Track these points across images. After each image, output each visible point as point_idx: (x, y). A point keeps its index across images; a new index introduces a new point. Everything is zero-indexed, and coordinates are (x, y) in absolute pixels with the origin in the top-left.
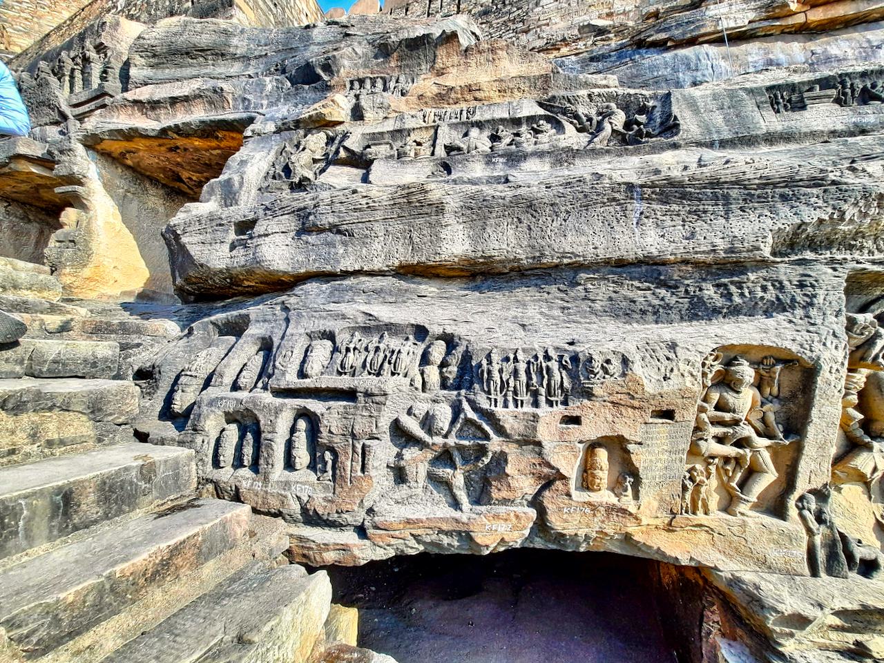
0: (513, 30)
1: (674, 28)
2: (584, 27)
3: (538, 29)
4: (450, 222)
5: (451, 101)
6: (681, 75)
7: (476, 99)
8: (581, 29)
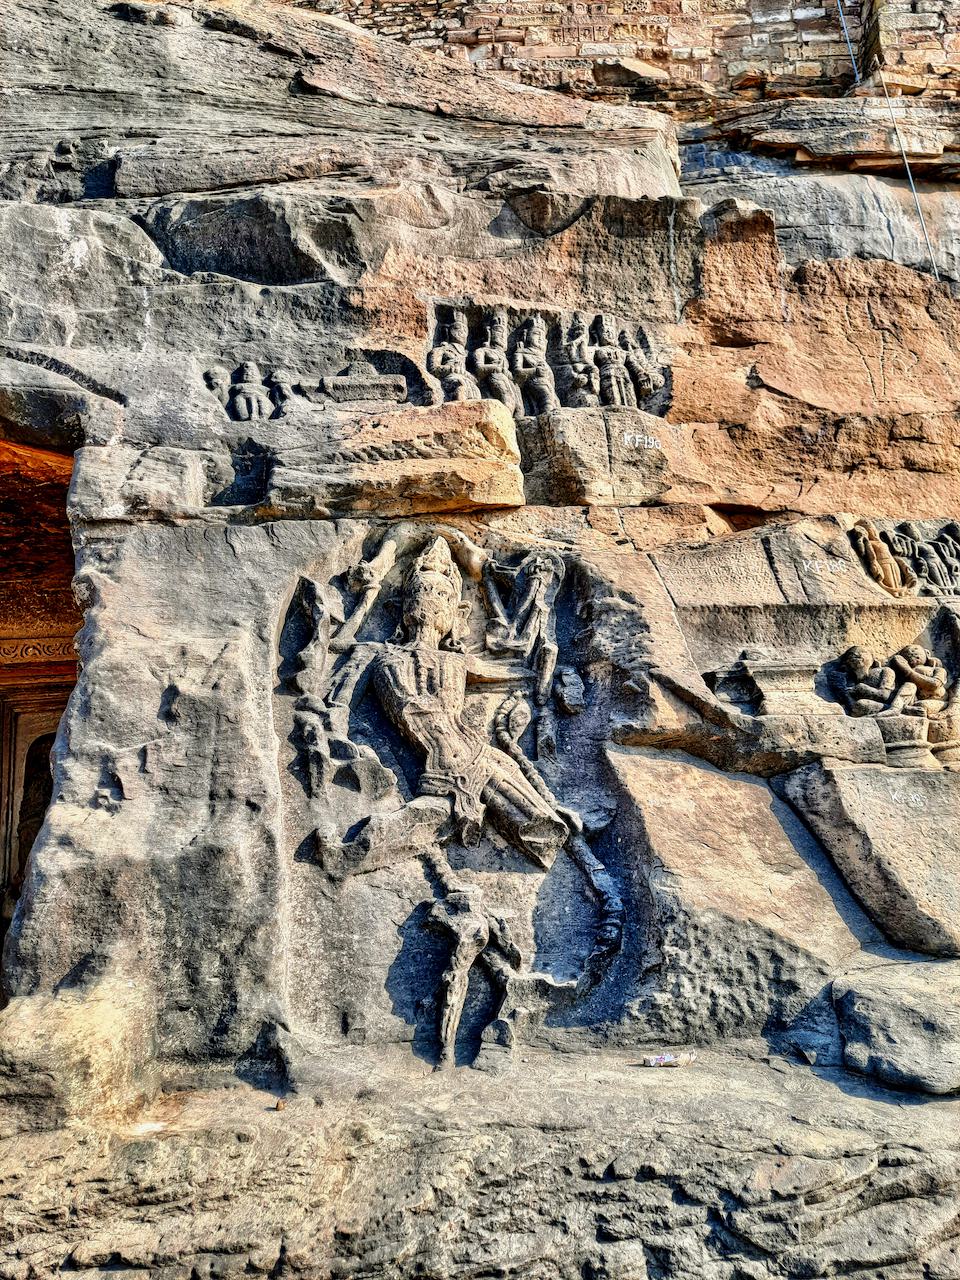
0: (438, 31)
1: (806, 125)
2: (605, 68)
3: (500, 47)
5: (837, 460)
6: (833, 233)
7: (910, 465)
8: (600, 70)
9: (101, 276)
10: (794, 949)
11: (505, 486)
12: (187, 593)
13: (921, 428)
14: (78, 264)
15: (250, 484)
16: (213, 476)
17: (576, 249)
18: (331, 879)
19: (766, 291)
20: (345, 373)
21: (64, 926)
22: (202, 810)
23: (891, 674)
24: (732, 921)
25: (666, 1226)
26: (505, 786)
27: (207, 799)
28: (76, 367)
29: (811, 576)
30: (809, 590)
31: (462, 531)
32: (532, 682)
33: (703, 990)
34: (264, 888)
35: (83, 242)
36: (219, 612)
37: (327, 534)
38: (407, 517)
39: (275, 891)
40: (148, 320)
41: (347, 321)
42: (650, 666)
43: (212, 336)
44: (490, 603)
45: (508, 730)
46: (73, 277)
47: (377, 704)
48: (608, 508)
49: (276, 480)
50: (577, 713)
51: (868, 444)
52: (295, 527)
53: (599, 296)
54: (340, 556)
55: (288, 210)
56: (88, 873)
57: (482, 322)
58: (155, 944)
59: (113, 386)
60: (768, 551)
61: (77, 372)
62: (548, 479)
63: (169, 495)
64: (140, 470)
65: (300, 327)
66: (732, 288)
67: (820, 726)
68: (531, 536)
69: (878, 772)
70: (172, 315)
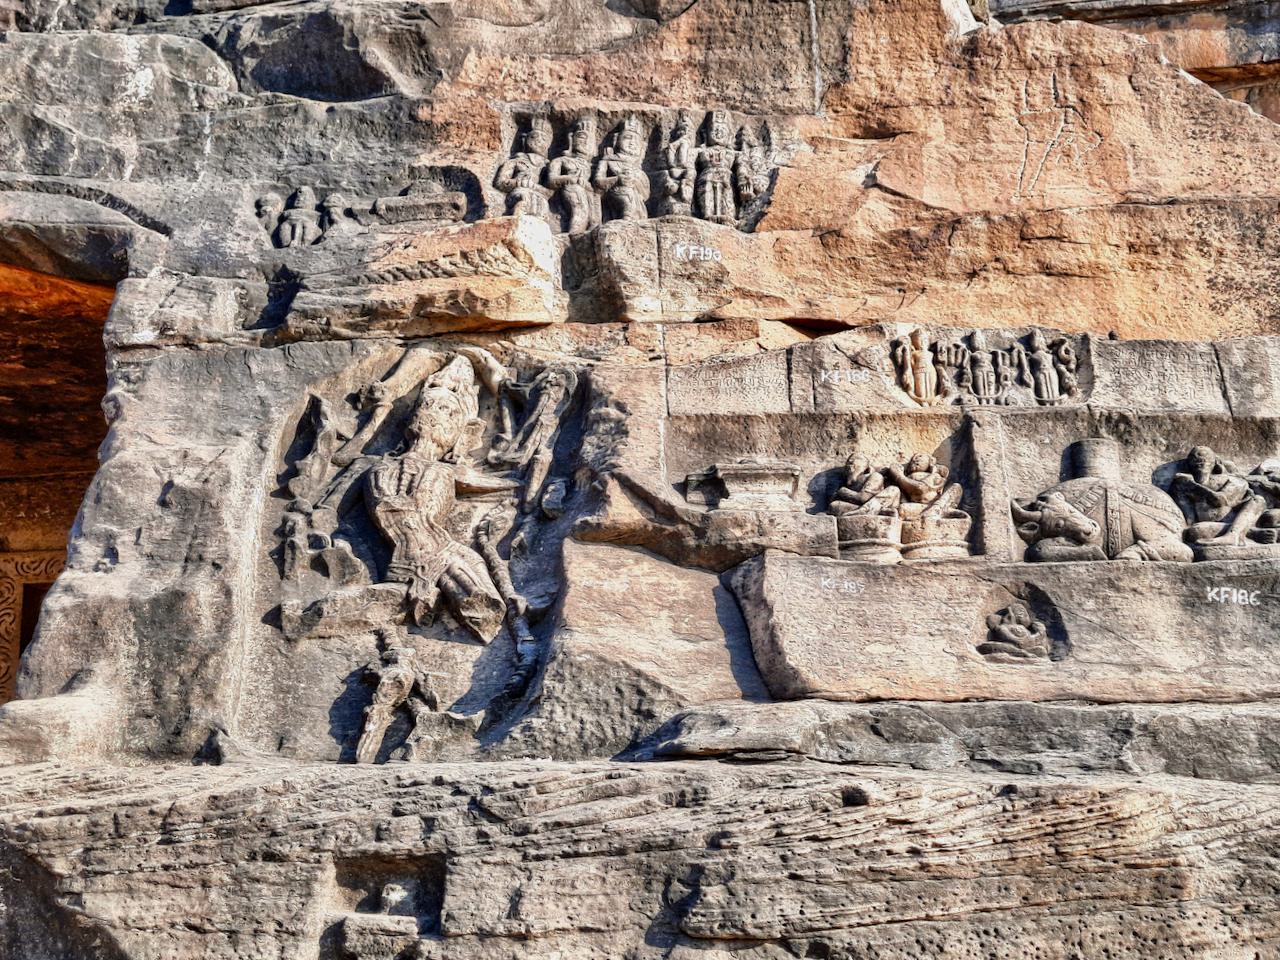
4: (1209, 933)
5: (951, 266)
7: (1047, 270)
9: (165, 104)
10: (657, 686)
11: (527, 302)
12: (199, 409)
13: (1059, 226)
14: (142, 93)
15: (277, 313)
16: (245, 303)
17: (697, 34)
18: (288, 640)
19: (928, 68)
20: (404, 193)
21: (62, 649)
22: (177, 569)
24: (605, 660)
25: (439, 806)
26: (458, 572)
27: (182, 563)
28: (129, 201)
29: (826, 386)
32: (521, 492)
33: (573, 716)
34: (219, 628)
35: (148, 71)
36: (224, 426)
37: (342, 354)
39: (228, 632)
40: (208, 147)
41: (415, 137)
42: (614, 466)
43: (271, 161)
45: (487, 534)
46: (136, 109)
47: (359, 511)
48: (650, 325)
49: (296, 304)
50: (554, 519)
51: (991, 246)
52: (311, 349)
53: (721, 86)
54: (355, 376)
55: (357, 22)
56: (81, 608)
57: (565, 129)
58: (129, 665)
60: (789, 362)
61: (130, 208)
62: (597, 296)
63: (195, 320)
64: (173, 299)
65: (365, 147)
66: (885, 68)
67: (771, 521)
68: (560, 354)
70: (232, 140)
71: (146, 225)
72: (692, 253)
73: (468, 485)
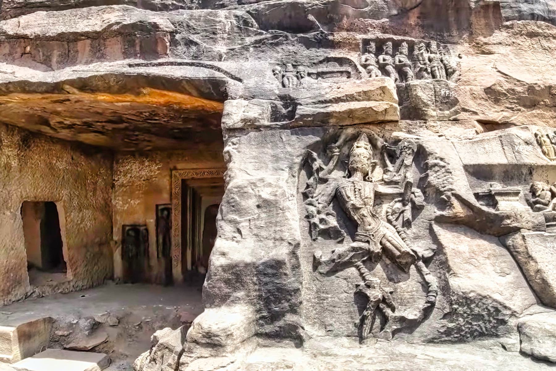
10: (506, 307)
23: (549, 194)
30: (518, 159)
31: (375, 131)
38: (351, 125)
44: (385, 161)
59: (238, 76)
61: (226, 72)
67: (521, 216)
69: (542, 235)
71: (233, 78)
72: (447, 93)
73: (380, 192)
